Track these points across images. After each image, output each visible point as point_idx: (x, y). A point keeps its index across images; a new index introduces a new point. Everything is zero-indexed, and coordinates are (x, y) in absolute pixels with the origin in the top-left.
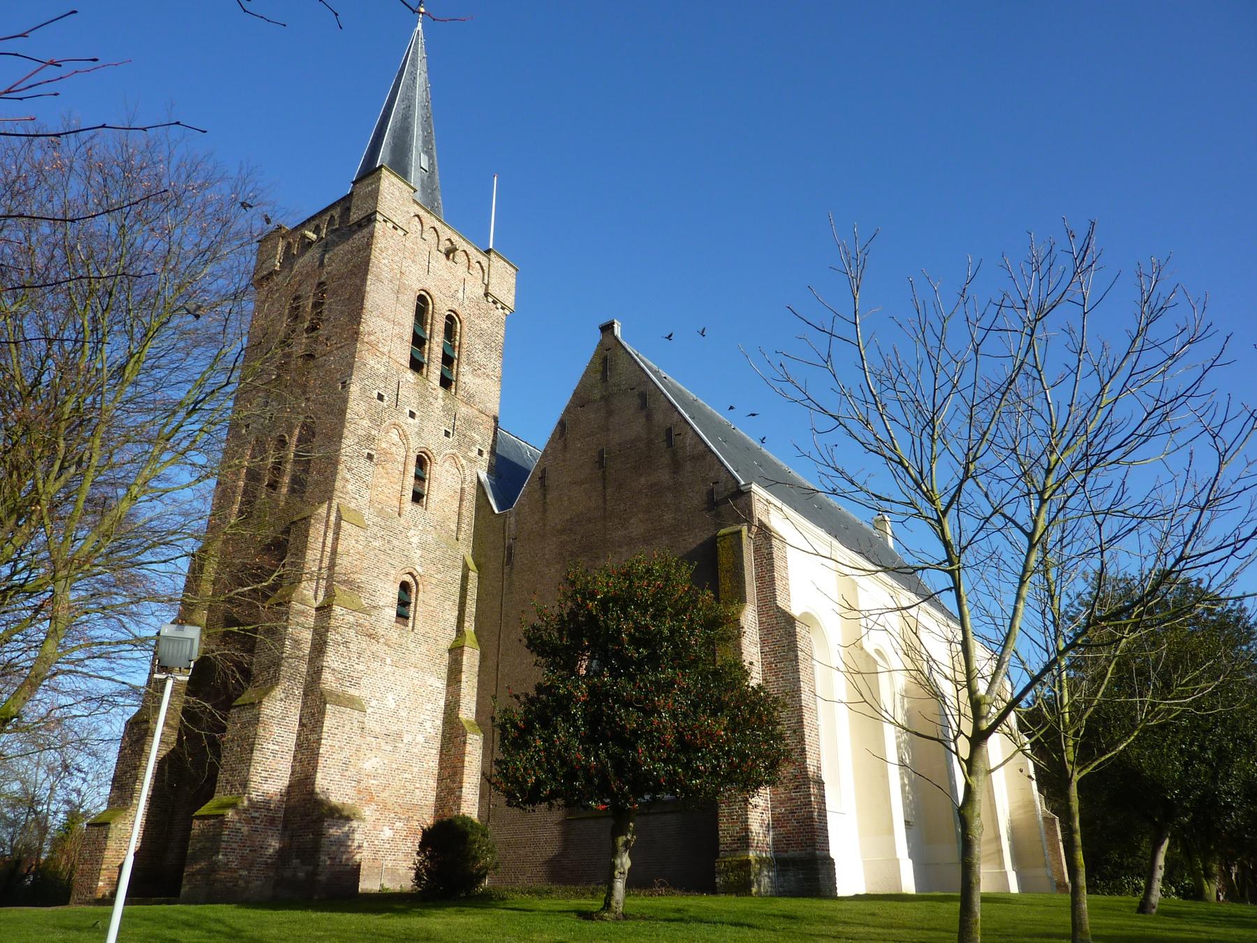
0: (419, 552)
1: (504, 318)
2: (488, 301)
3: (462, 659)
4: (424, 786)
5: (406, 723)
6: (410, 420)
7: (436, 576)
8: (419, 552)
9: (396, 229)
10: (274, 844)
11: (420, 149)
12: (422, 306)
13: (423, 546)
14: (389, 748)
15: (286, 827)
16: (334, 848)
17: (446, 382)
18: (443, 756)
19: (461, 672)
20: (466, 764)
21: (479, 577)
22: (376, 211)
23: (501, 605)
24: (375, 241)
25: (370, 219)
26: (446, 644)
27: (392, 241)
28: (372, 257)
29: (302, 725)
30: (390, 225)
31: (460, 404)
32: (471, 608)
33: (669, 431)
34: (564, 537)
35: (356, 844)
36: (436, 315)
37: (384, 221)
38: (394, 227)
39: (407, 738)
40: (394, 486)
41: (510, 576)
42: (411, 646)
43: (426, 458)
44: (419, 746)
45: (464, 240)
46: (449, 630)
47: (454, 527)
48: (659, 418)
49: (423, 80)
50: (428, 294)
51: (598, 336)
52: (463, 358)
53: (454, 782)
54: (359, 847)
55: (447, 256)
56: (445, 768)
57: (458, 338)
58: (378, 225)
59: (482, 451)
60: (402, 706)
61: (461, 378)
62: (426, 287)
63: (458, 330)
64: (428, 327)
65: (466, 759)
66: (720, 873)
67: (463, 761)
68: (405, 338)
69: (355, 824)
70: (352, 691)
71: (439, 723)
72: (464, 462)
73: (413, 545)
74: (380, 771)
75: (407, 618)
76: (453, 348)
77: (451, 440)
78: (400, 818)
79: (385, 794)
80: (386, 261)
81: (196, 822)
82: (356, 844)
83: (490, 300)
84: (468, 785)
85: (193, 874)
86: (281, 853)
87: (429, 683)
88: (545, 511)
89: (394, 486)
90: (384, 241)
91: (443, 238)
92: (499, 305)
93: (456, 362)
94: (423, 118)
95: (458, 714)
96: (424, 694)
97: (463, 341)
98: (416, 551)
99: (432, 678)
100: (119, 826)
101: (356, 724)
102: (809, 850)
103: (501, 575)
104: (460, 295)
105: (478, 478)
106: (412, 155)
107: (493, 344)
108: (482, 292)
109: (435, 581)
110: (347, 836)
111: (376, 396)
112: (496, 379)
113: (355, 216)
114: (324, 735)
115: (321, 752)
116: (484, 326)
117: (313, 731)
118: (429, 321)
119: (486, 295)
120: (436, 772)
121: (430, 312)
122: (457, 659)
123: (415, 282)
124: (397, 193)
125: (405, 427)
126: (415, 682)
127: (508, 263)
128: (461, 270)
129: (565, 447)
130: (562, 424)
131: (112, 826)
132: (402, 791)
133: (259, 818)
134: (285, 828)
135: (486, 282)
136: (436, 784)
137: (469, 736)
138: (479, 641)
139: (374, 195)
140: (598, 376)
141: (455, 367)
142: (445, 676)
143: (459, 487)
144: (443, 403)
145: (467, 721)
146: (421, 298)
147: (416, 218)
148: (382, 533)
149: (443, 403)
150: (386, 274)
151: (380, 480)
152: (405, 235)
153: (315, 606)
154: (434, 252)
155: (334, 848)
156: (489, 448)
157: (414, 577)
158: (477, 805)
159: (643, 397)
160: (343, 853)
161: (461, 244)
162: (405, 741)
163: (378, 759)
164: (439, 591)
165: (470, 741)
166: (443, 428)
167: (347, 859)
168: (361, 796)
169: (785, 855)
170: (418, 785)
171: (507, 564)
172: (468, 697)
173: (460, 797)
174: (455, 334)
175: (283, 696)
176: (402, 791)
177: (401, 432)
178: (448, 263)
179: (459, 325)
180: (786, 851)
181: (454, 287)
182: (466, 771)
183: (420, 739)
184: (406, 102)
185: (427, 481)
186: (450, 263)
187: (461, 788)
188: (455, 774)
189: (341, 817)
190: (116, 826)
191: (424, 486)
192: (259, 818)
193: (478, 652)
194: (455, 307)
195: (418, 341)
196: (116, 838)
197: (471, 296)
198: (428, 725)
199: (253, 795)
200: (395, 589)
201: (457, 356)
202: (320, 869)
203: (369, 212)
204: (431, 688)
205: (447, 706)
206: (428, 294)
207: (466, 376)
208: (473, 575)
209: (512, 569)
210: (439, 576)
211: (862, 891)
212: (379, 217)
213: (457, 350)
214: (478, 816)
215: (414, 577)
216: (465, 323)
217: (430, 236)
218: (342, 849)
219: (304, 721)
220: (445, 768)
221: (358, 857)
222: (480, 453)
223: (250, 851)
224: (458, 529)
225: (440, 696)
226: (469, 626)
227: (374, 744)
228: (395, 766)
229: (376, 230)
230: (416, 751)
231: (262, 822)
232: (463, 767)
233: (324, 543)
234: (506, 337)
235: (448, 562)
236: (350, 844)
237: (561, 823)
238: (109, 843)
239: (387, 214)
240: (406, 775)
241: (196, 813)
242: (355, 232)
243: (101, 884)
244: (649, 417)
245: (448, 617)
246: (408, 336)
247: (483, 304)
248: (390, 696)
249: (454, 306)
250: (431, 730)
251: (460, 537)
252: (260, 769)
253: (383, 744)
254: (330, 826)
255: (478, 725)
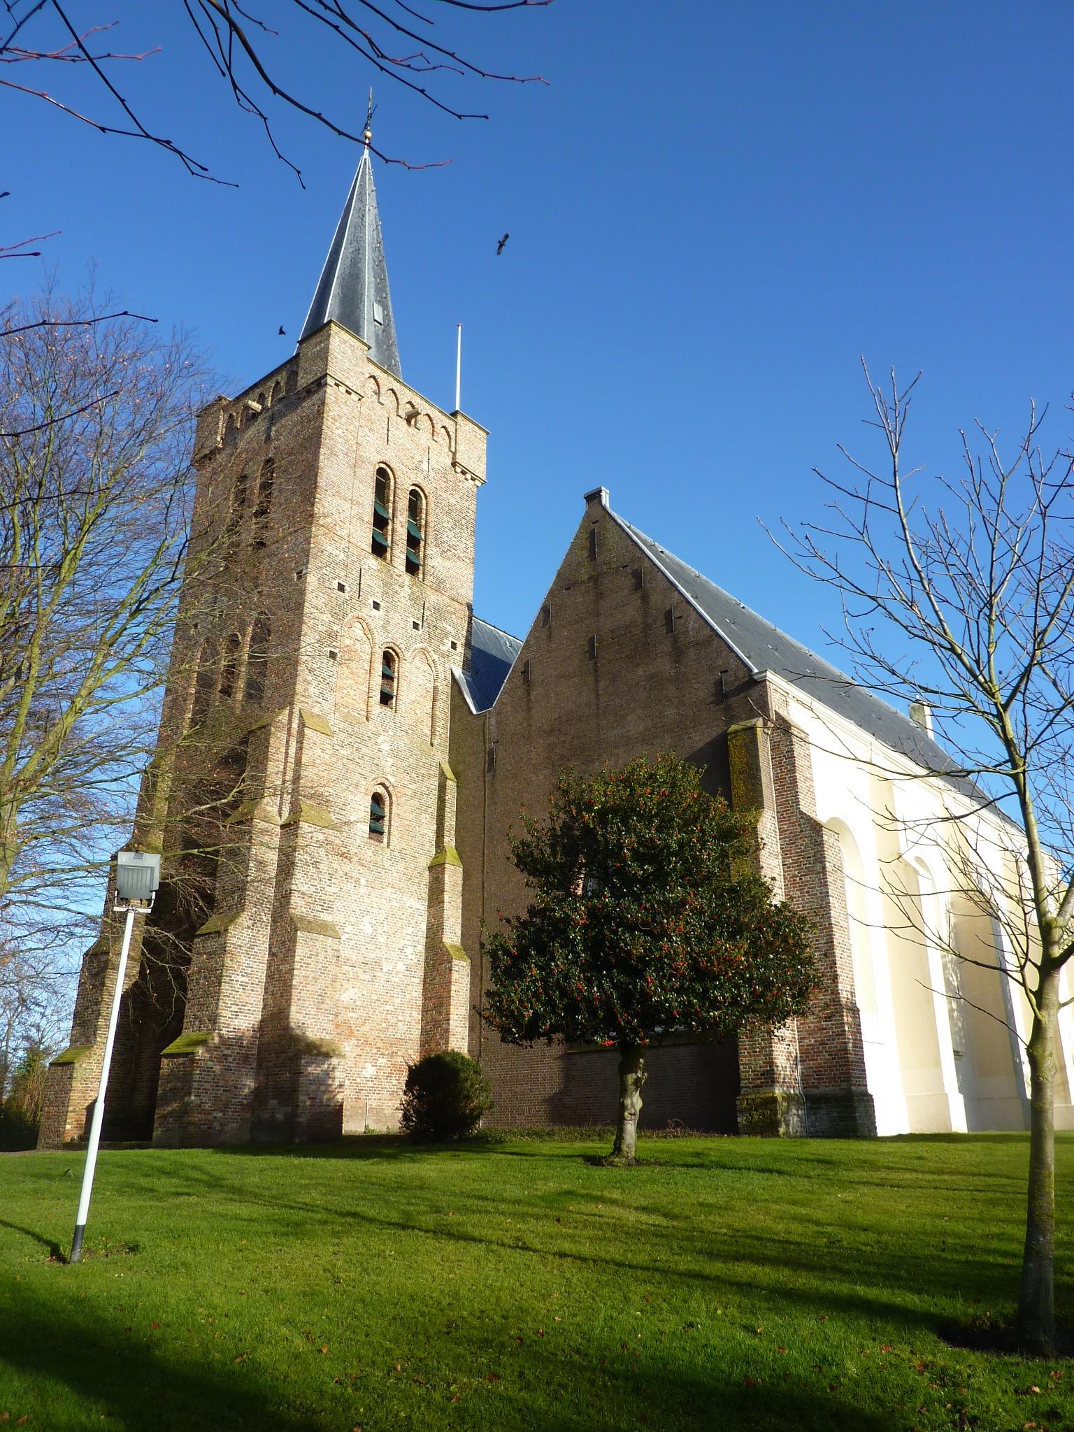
0: (391, 761)
1: (475, 490)
2: (456, 472)
3: (444, 877)
4: (408, 1019)
5: (384, 949)
6: (375, 612)
7: (410, 786)
8: (391, 761)
9: (350, 394)
10: (249, 1084)
11: (373, 298)
12: (383, 479)
13: (395, 753)
14: (367, 977)
15: (261, 1065)
16: (313, 1087)
17: (412, 568)
18: (427, 985)
19: (443, 891)
20: (453, 993)
21: (458, 787)
22: (326, 374)
23: (484, 817)
24: (326, 408)
25: (319, 384)
26: (425, 861)
27: (345, 408)
28: (324, 427)
29: (271, 954)
30: (342, 389)
31: (429, 591)
32: (451, 821)
33: (668, 614)
34: (552, 739)
35: (337, 1083)
36: (398, 491)
37: (336, 384)
38: (347, 391)
39: (386, 966)
40: (360, 687)
41: (492, 785)
42: (388, 864)
43: (394, 654)
44: (400, 975)
45: (426, 402)
46: (427, 847)
47: (427, 731)
48: (655, 599)
49: (372, 217)
50: (389, 466)
51: (583, 507)
52: (431, 539)
53: (440, 1013)
54: (341, 1086)
55: (409, 422)
56: (430, 999)
57: (423, 516)
58: (329, 390)
59: (455, 644)
60: (380, 931)
61: (428, 561)
62: (386, 459)
63: (424, 507)
64: (391, 505)
65: (453, 988)
66: (743, 1111)
67: (450, 991)
68: (366, 519)
69: (334, 1061)
70: (325, 917)
71: (421, 948)
72: (436, 657)
73: (384, 752)
74: (358, 1003)
75: (382, 833)
76: (419, 527)
77: (420, 632)
78: (382, 1054)
79: (366, 1028)
80: (339, 431)
81: (165, 1061)
82: (337, 1083)
83: (459, 470)
84: (456, 1017)
85: (165, 1117)
86: (256, 1092)
87: (408, 905)
88: (530, 709)
89: (360, 687)
90: (337, 409)
91: (403, 401)
92: (468, 476)
93: (422, 543)
94: (374, 261)
95: (442, 938)
96: (404, 917)
97: (430, 519)
98: (387, 759)
99: (412, 899)
100: (84, 1065)
101: (330, 952)
102: (844, 1085)
103: (482, 784)
104: (425, 466)
105: (452, 674)
106: (364, 306)
107: (464, 521)
108: (449, 461)
109: (409, 792)
110: (327, 1074)
111: (336, 586)
112: (468, 561)
113: (303, 381)
114: (297, 965)
115: (294, 983)
116: (452, 501)
117: (284, 961)
118: (391, 498)
119: (454, 464)
120: (420, 1003)
121: (392, 488)
122: (438, 877)
123: (373, 456)
124: (349, 352)
125: (369, 620)
126: (394, 903)
127: (477, 426)
128: (424, 437)
129: (550, 636)
130: (545, 610)
131: (77, 1065)
132: (384, 1025)
133: (231, 1056)
134: (260, 1065)
135: (453, 449)
136: (420, 1017)
137: (455, 962)
138: (461, 858)
139: (324, 356)
140: (585, 553)
141: (422, 549)
142: (426, 896)
143: (431, 685)
144: (410, 591)
145: (452, 946)
146: (381, 472)
147: (372, 379)
148: (350, 740)
149: (410, 591)
150: (340, 447)
151: (344, 681)
152: (360, 400)
153: (280, 823)
154: (394, 418)
155: (313, 1087)
156: (463, 641)
157: (386, 788)
158: (467, 1038)
159: (637, 575)
160: (324, 1092)
161: (423, 407)
162: (385, 970)
163: (356, 990)
164: (415, 802)
165: (457, 969)
166: (411, 620)
167: (329, 1099)
168: (339, 1031)
169: (816, 1091)
170: (400, 1018)
171: (489, 771)
172: (452, 919)
173: (447, 1031)
174: (421, 512)
175: (250, 923)
176: (384, 1025)
177: (365, 626)
178: (410, 430)
179: (424, 501)
180: (817, 1087)
181: (418, 458)
182: (453, 1002)
183: (401, 967)
184: (355, 243)
185: (396, 680)
186: (412, 430)
187: (449, 1020)
188: (441, 1004)
189: (320, 1054)
190: (81, 1066)
191: (392, 686)
192: (231, 1056)
193: (461, 870)
194: (419, 481)
195: (380, 522)
196: (82, 1078)
197: (436, 467)
198: (409, 950)
199: (224, 1032)
200: (368, 801)
201: (423, 536)
202: (300, 1110)
203: (319, 375)
204: (411, 910)
205: (429, 929)
206: (389, 466)
207: (434, 559)
208: (451, 785)
209: (494, 776)
210: (413, 787)
211: (905, 1131)
212: (329, 380)
213: (423, 530)
214: (469, 1050)
215: (386, 788)
216: (431, 499)
217: (387, 399)
218: (323, 1088)
219: (274, 950)
220: (430, 999)
221: (339, 1097)
222: (454, 646)
223: (224, 1091)
224: (432, 733)
225: (421, 918)
226: (450, 841)
227: (351, 973)
228: (375, 997)
229: (327, 395)
230: (397, 980)
231: (235, 1060)
232: (450, 997)
233: (287, 754)
234: (477, 512)
235: (423, 771)
236: (330, 1082)
237: (560, 1057)
238: (74, 1084)
239: (339, 376)
240: (387, 1007)
241: (165, 1051)
242: (303, 400)
243: (68, 1127)
244: (645, 599)
245: (426, 831)
246: (369, 517)
247: (451, 476)
248: (366, 920)
249: (418, 479)
250: (413, 957)
251: (435, 742)
252: (230, 1002)
253: (360, 972)
254: (308, 1064)
255: (464, 950)
